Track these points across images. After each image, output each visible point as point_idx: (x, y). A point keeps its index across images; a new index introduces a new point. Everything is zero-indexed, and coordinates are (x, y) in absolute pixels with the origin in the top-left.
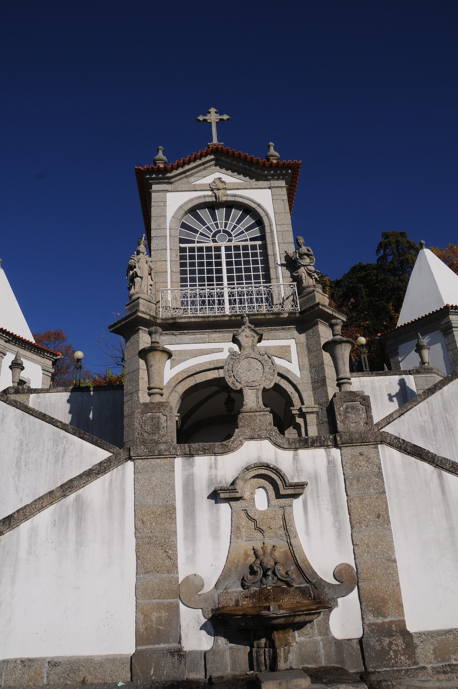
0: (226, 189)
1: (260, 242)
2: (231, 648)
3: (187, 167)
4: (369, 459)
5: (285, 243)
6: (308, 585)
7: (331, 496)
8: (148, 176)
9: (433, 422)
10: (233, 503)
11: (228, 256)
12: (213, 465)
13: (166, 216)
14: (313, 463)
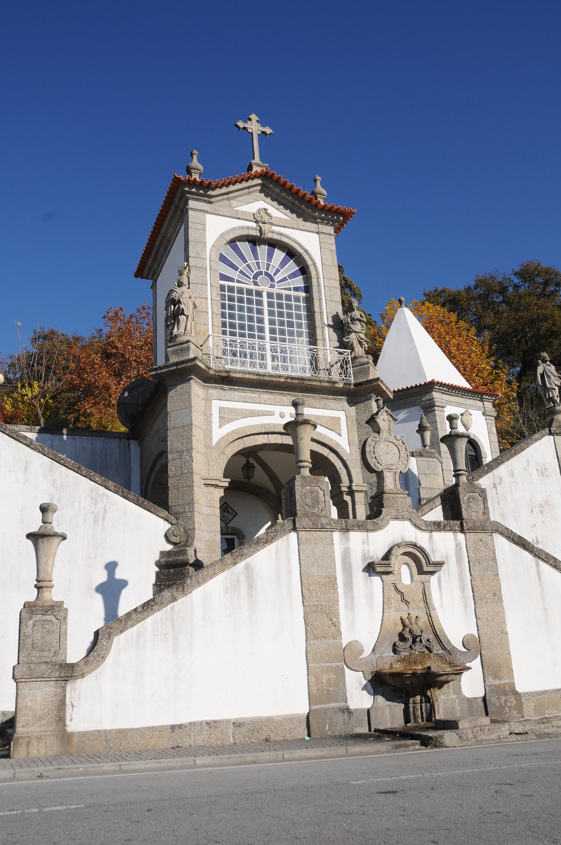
0: (271, 224)
2: (389, 705)
3: (231, 188)
4: (487, 545)
5: (332, 301)
6: (443, 651)
7: (459, 575)
8: (187, 189)
10: (384, 577)
12: (366, 541)
13: (205, 243)
14: (444, 545)
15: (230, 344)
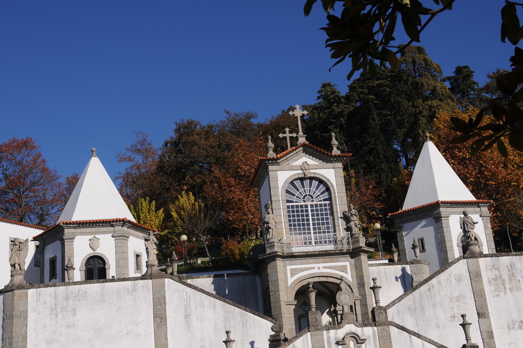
1: (328, 202)
9: (414, 305)
11: (312, 211)
14: (368, 332)
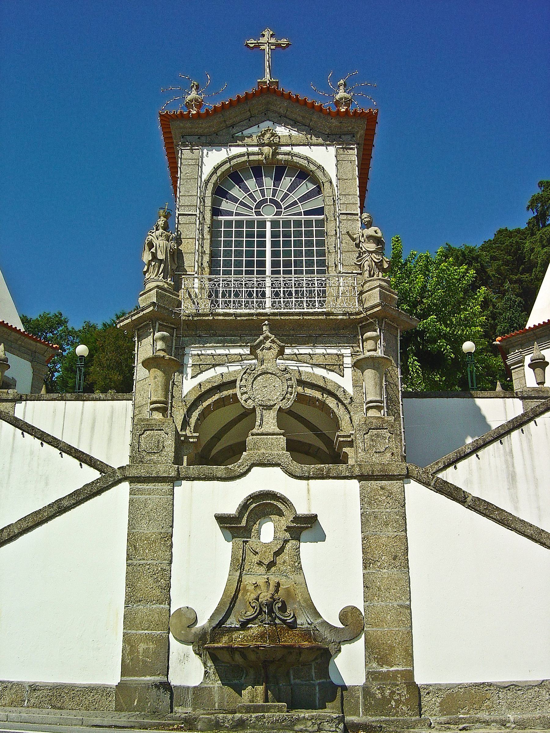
11: (274, 235)
15: (245, 284)
